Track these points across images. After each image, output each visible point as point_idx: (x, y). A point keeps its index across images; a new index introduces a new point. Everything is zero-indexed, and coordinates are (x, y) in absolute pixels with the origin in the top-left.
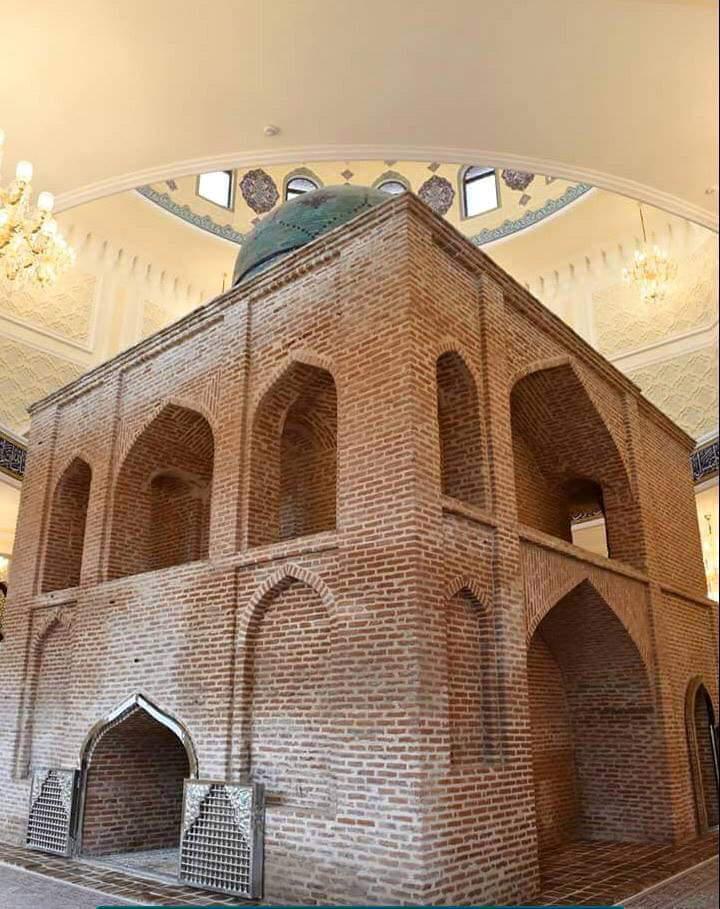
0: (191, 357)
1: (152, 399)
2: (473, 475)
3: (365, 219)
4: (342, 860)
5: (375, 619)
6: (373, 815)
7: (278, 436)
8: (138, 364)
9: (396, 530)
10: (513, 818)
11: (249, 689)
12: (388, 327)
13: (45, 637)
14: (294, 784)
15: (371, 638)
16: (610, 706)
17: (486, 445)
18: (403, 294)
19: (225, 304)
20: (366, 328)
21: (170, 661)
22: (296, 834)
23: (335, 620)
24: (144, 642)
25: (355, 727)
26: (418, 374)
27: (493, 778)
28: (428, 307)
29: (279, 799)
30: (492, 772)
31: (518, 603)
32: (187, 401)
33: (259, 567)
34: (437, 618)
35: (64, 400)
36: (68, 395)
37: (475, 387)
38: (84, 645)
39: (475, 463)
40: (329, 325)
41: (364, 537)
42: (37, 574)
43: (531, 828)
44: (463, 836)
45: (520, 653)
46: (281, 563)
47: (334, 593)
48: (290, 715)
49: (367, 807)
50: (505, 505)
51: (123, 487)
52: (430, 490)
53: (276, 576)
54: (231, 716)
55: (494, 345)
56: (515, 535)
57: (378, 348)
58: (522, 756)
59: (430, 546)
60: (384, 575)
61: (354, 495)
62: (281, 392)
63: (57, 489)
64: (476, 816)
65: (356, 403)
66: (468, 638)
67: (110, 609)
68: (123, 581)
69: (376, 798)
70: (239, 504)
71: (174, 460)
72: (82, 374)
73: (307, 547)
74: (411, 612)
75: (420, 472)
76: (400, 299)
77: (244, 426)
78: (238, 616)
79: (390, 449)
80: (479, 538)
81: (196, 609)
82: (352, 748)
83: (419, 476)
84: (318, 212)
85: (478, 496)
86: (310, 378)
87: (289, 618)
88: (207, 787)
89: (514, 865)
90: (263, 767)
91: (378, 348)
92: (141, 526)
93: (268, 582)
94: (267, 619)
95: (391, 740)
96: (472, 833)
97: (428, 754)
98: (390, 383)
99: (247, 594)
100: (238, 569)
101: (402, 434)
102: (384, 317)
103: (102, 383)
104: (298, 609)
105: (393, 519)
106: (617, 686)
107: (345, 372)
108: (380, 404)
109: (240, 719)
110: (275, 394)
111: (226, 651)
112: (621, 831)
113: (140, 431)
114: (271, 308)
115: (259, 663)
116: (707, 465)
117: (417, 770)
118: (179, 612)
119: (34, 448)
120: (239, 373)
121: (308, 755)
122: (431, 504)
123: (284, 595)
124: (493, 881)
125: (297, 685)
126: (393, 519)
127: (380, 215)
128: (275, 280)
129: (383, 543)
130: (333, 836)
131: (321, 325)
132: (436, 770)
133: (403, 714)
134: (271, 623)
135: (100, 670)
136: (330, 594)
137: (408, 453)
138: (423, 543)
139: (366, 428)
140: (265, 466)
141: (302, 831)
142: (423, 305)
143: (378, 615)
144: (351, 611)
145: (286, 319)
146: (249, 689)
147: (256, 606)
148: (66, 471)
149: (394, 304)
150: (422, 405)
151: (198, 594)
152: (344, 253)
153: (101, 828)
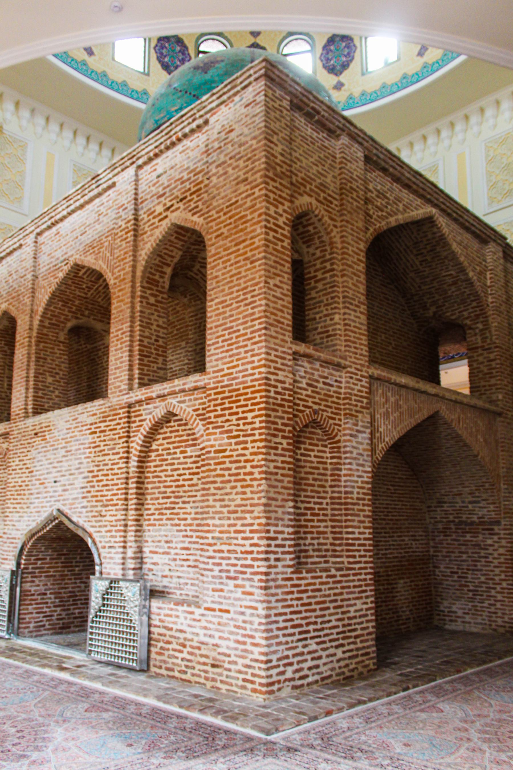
0: (91, 220)
1: (62, 259)
2: (329, 322)
3: (229, 87)
4: (206, 640)
5: (234, 447)
6: (229, 604)
7: (165, 290)
8: (49, 228)
9: (250, 372)
10: (352, 609)
11: (140, 505)
14: (175, 580)
15: (231, 462)
16: (464, 519)
18: (259, 159)
19: (116, 171)
20: (229, 191)
21: (80, 482)
22: (173, 619)
23: (203, 449)
25: (217, 535)
26: (272, 234)
27: (334, 576)
28: (284, 170)
29: (163, 592)
30: (333, 572)
31: (364, 432)
32: (90, 261)
34: (285, 446)
37: (331, 243)
39: (330, 312)
40: (200, 189)
41: (225, 378)
43: (370, 618)
44: (304, 622)
45: (365, 475)
46: (163, 401)
47: (204, 425)
48: (172, 525)
49: (225, 598)
50: (355, 348)
51: (41, 338)
52: (281, 337)
53: (158, 410)
54: (126, 525)
58: (363, 559)
59: (279, 385)
60: (240, 410)
64: (318, 607)
65: (220, 261)
66: (318, 462)
68: (43, 416)
69: (231, 591)
70: (130, 351)
71: (87, 312)
73: (182, 387)
74: (261, 441)
75: (271, 321)
76: (257, 163)
77: (133, 281)
78: (131, 445)
79: (247, 302)
82: (215, 551)
86: (189, 238)
87: (171, 446)
88: (107, 583)
89: (352, 647)
90: (152, 567)
94: (154, 447)
95: (244, 545)
96: (313, 620)
97: (272, 556)
98: (248, 243)
100: (130, 406)
101: (256, 288)
103: (21, 245)
104: (178, 439)
105: (248, 363)
106: (470, 502)
109: (133, 528)
110: (159, 253)
112: (469, 623)
113: (53, 288)
114: (155, 174)
117: (264, 570)
121: (185, 557)
122: (280, 349)
124: (331, 659)
125: (177, 500)
126: (248, 363)
129: (240, 383)
130: (199, 621)
131: (193, 190)
132: (280, 569)
133: (252, 525)
134: (157, 450)
136: (200, 426)
137: (261, 305)
138: (273, 383)
140: (153, 317)
141: (177, 617)
142: (278, 168)
143: (236, 444)
144: (215, 440)
145: (166, 184)
146: (140, 505)
147: (145, 437)
149: (252, 169)
150: (275, 262)
152: (212, 121)
153: (35, 615)
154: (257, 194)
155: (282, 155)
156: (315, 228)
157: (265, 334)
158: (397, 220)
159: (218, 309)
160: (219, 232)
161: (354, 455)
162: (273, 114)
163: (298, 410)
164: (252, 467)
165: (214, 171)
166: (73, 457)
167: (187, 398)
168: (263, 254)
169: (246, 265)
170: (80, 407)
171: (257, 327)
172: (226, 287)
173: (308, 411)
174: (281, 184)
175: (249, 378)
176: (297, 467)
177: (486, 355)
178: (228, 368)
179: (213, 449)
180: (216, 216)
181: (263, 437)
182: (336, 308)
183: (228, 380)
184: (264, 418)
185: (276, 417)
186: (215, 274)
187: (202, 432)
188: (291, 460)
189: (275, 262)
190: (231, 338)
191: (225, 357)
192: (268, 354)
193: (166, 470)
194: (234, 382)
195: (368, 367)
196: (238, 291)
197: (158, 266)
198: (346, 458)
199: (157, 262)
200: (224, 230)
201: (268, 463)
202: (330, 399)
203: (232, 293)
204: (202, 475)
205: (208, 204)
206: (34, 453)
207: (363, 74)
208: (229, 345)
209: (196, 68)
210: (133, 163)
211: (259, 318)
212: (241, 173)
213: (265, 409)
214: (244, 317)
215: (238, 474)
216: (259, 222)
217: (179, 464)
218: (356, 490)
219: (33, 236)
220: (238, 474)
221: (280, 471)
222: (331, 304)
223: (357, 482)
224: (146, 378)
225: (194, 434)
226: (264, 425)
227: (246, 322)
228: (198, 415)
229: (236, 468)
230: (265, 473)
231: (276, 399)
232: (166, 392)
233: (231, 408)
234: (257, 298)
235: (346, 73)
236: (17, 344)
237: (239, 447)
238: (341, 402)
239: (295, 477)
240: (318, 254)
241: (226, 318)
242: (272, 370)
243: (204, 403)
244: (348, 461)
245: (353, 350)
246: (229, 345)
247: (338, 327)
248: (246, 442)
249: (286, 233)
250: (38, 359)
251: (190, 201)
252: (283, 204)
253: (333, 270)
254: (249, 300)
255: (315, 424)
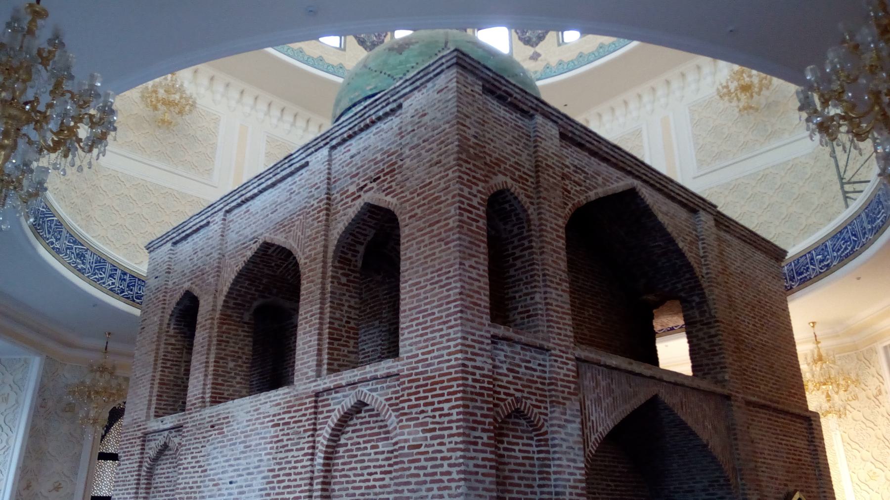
0: (282, 198)
2: (529, 302)
3: (422, 74)
5: (429, 442)
8: (239, 205)
9: (446, 358)
12: (441, 172)
13: (155, 460)
15: (426, 460)
17: (540, 273)
18: (452, 143)
19: (309, 151)
23: (396, 443)
24: (238, 465)
26: (466, 214)
28: (477, 152)
31: (574, 422)
32: (279, 239)
33: (336, 392)
34: (485, 440)
35: (177, 238)
36: (180, 235)
37: (529, 221)
38: (187, 468)
39: (530, 290)
41: (420, 365)
42: (150, 401)
45: (578, 472)
46: (354, 389)
47: (397, 417)
51: (225, 318)
52: (477, 320)
53: (348, 400)
55: (549, 181)
56: (572, 357)
57: (432, 191)
59: (478, 372)
60: (436, 400)
61: (412, 326)
62: (358, 230)
63: (170, 320)
65: (414, 242)
66: (524, 458)
67: (210, 433)
70: (319, 334)
72: (191, 215)
73: (373, 374)
74: (459, 435)
75: (467, 304)
77: (325, 262)
78: (317, 439)
79: (442, 284)
80: (532, 361)
81: (282, 433)
83: (466, 307)
84: (402, 57)
85: (533, 321)
87: (361, 440)
91: (432, 191)
92: (243, 353)
93: (343, 407)
94: (342, 441)
99: (325, 418)
100: (317, 394)
101: (451, 269)
102: (437, 163)
103: (208, 223)
104: (369, 432)
107: (406, 214)
108: (434, 242)
111: (306, 473)
113: (240, 267)
114: (348, 155)
115: (335, 483)
116: (802, 273)
118: (268, 435)
119: (152, 283)
120: (321, 214)
122: (478, 333)
123: (357, 418)
127: (434, 70)
128: (350, 129)
131: (387, 171)
134: (346, 445)
135: (200, 492)
136: (393, 418)
137: (456, 288)
138: (470, 369)
139: (422, 264)
140: (344, 298)
142: (472, 151)
143: (432, 438)
144: (409, 434)
145: (360, 165)
147: (333, 429)
148: (178, 304)
149: (446, 152)
150: (470, 242)
151: (284, 419)
152: (405, 105)
154: (451, 175)
155: (475, 137)
156: (511, 206)
157: (461, 318)
158: (596, 194)
159: (412, 291)
160: (413, 213)
161: (564, 449)
162: (465, 99)
163: (498, 399)
164: (450, 465)
165: (408, 152)
166: (252, 453)
167: (379, 386)
168: (457, 236)
169: (441, 246)
170: (263, 396)
171: (452, 310)
172: (421, 269)
173: (510, 399)
174: (474, 165)
175: (445, 365)
176: (499, 464)
177: (706, 330)
178: (423, 354)
179: (406, 445)
180: (409, 197)
181: (461, 431)
182: (535, 287)
183: (423, 367)
184: (461, 409)
185: (474, 407)
186: (409, 255)
187: (395, 424)
188: (493, 456)
189: (470, 242)
190: (426, 322)
191: (420, 342)
192: (464, 338)
193: (356, 469)
194: (429, 369)
195: (574, 349)
196: (432, 273)
197: (351, 245)
198: (555, 452)
199: (349, 241)
200: (418, 211)
201: (467, 461)
202: (534, 385)
203: (427, 274)
204: (394, 474)
205: (401, 184)
206: (209, 448)
207: (559, 45)
208: (423, 329)
209: (391, 49)
210: (327, 143)
211: (455, 301)
212: (434, 156)
213: (462, 399)
214: (439, 300)
215: (435, 474)
216: (454, 203)
217: (369, 461)
218: (568, 491)
219: (221, 214)
220: (435, 474)
221: (481, 470)
222: (531, 282)
223: (569, 480)
224: (336, 363)
225: (386, 426)
226: (461, 417)
227: (441, 305)
228: (390, 405)
229: (432, 467)
230: (464, 472)
231: (475, 387)
232: (356, 379)
233: (427, 397)
234: (451, 280)
235: (542, 44)
236: (198, 326)
237: (436, 442)
238: (546, 388)
239: (498, 476)
240: (516, 231)
241: (420, 300)
242: (469, 356)
243: (397, 392)
244: (557, 456)
245: (556, 330)
246: (423, 329)
247: (540, 306)
248: (442, 437)
249: (481, 213)
250: (220, 342)
251: (384, 181)
252: (477, 185)
253: (532, 247)
254: (444, 282)
255: (518, 413)
